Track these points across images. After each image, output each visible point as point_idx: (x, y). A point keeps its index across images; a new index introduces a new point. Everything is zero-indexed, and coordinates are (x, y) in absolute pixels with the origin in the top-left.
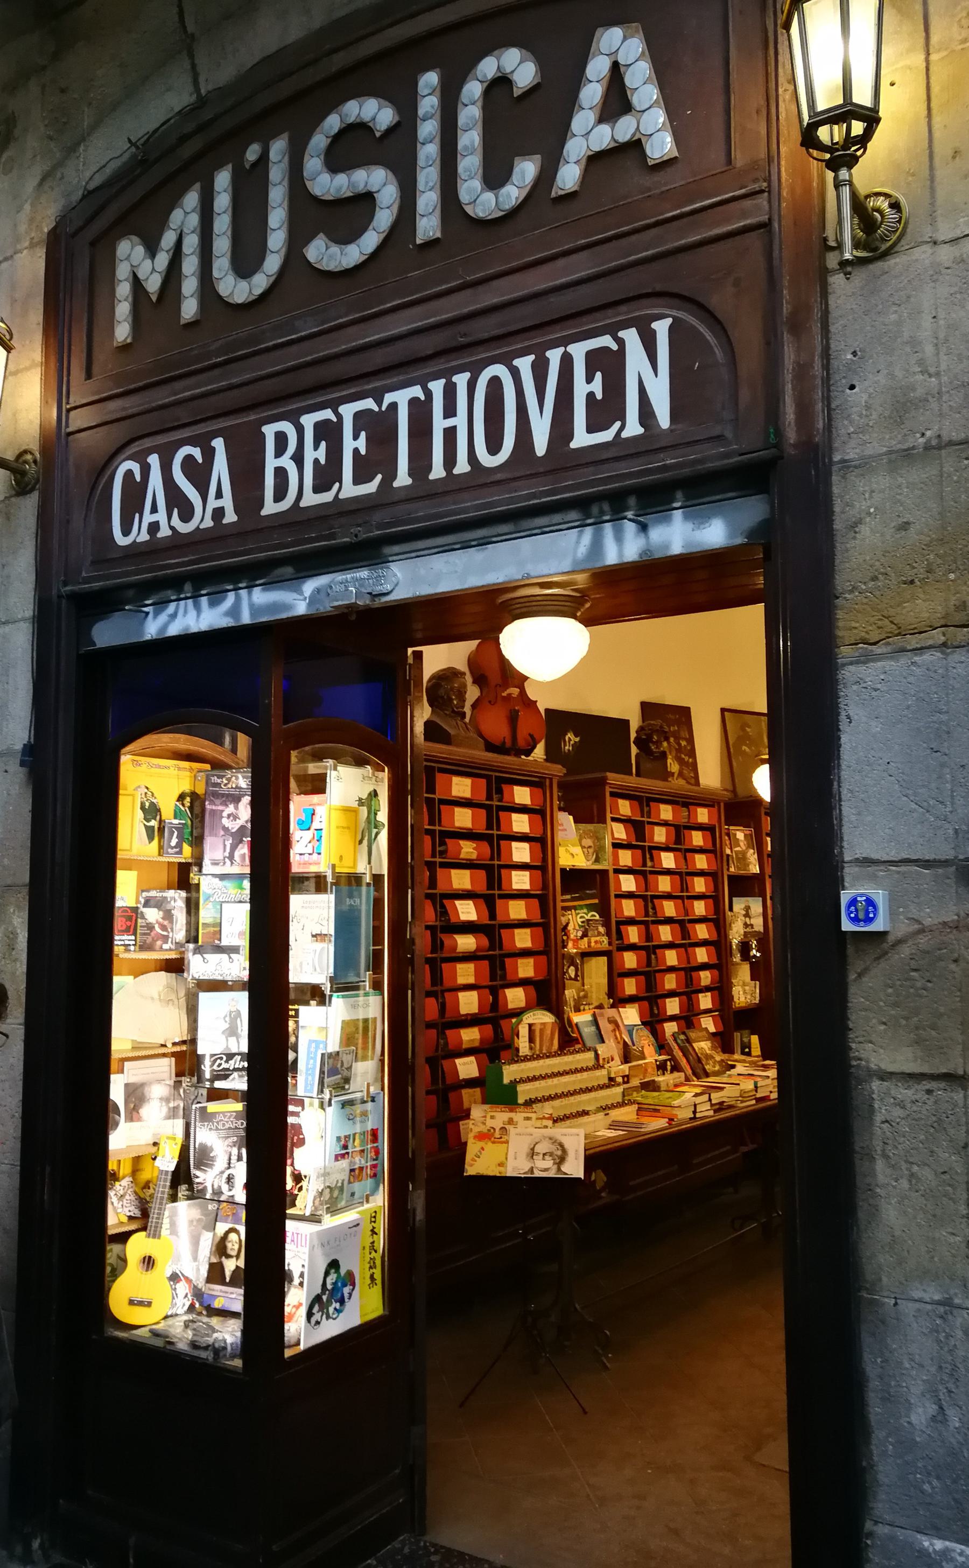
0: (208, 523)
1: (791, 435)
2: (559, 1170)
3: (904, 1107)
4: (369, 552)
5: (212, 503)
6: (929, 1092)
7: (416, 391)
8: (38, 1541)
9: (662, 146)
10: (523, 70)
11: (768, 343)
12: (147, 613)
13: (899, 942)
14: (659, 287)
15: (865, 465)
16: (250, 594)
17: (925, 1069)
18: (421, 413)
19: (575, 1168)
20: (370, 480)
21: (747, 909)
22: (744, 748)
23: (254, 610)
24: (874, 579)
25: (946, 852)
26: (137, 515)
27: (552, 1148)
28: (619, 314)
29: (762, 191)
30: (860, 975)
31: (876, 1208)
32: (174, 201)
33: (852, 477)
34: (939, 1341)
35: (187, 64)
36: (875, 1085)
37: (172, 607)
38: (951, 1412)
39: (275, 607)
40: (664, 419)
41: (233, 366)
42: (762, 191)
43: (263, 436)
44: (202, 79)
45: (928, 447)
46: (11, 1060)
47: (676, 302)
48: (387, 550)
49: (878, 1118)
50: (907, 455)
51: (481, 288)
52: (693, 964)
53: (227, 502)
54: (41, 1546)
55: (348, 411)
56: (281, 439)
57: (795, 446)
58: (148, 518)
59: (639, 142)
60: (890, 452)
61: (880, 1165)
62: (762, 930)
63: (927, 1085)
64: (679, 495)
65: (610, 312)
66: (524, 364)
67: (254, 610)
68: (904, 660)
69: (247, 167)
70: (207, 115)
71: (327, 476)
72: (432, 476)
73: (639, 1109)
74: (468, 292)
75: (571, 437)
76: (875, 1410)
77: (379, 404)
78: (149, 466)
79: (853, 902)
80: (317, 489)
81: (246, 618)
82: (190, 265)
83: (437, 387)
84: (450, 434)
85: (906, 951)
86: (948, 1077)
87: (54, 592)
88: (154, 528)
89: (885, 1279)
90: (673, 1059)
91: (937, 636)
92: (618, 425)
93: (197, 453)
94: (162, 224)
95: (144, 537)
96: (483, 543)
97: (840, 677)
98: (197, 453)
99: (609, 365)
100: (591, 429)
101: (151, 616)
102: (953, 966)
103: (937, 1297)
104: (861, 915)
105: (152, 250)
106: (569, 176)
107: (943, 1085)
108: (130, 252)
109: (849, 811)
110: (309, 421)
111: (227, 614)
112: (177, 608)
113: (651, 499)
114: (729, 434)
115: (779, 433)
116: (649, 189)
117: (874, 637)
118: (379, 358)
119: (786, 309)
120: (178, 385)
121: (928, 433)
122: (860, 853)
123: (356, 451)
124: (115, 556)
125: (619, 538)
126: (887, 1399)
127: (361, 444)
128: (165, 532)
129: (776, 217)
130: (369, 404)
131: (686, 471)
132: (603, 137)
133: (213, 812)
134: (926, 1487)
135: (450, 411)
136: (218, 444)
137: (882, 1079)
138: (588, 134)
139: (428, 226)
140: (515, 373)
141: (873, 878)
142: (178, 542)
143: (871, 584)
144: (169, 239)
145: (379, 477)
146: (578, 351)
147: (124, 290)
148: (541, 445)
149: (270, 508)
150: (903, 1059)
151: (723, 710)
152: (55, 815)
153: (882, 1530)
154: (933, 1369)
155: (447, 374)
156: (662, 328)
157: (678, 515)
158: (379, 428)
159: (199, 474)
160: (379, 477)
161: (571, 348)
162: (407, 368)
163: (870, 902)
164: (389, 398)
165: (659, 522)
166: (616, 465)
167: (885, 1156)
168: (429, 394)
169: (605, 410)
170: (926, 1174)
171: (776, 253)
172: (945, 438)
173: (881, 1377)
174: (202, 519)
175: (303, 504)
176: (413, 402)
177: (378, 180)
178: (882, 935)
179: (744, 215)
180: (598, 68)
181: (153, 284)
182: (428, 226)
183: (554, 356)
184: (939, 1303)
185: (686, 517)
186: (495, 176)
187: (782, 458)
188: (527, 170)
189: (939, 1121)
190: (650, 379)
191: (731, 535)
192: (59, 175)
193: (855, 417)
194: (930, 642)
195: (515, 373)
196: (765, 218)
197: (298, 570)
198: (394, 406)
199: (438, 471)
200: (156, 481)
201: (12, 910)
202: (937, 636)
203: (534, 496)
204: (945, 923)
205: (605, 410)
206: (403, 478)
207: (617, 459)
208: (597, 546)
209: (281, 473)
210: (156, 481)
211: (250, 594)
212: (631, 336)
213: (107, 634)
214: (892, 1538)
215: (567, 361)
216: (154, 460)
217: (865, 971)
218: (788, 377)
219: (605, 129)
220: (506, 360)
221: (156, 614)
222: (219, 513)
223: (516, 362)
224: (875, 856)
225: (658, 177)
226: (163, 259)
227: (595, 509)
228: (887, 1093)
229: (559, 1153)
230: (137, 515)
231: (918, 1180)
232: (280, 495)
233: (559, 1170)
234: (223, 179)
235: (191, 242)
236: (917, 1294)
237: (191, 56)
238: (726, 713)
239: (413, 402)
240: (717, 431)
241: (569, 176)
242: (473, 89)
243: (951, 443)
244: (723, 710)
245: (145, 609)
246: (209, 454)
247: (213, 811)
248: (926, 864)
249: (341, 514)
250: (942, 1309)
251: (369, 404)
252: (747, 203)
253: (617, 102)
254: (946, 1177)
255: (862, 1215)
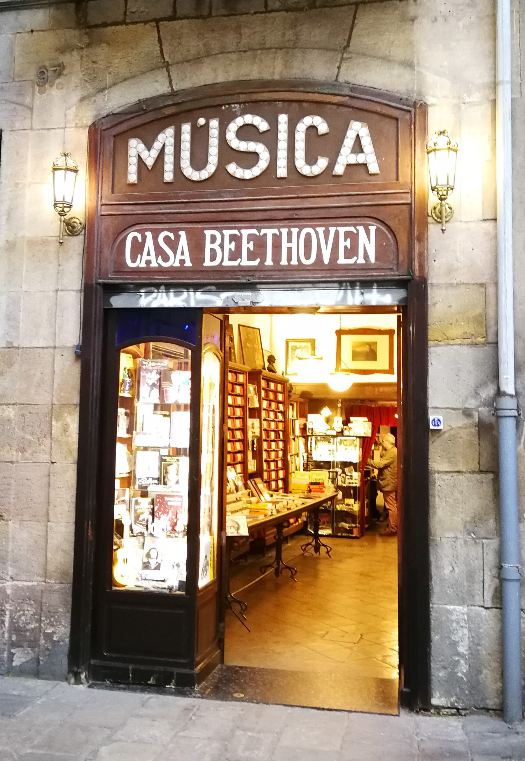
0: (177, 264)
1: (417, 273)
2: (238, 533)
3: (445, 481)
4: (251, 286)
5: (179, 257)
6: (452, 476)
7: (276, 231)
8: (84, 674)
9: (374, 168)
10: (323, 128)
11: (409, 242)
12: (141, 296)
13: (445, 432)
14: (372, 215)
15: (438, 286)
16: (195, 295)
17: (451, 470)
18: (277, 239)
19: (245, 532)
20: (255, 260)
21: (253, 424)
22: (248, 344)
23: (197, 301)
24: (441, 321)
25: (459, 406)
26: (139, 256)
27: (234, 524)
28: (357, 221)
29: (408, 193)
30: (433, 442)
31: (435, 512)
32: (161, 129)
33: (434, 288)
34: (453, 549)
35: (166, 74)
36: (436, 475)
37: (154, 295)
38: (456, 569)
39: (206, 301)
40: (372, 260)
41: (191, 204)
42: (408, 193)
43: (204, 235)
44: (174, 83)
45: (457, 284)
46: (66, 478)
47: (378, 221)
48: (258, 286)
49: (437, 485)
50: (451, 285)
51: (305, 199)
52: (236, 451)
53: (187, 257)
54: (86, 676)
55: (245, 233)
56: (213, 239)
57: (419, 277)
58: (145, 257)
59: (366, 164)
60: (446, 284)
61: (437, 499)
62: (259, 435)
63: (452, 474)
64: (375, 284)
65: (354, 219)
66: (321, 230)
67: (197, 301)
68: (449, 347)
69: (199, 127)
70: (178, 100)
71: (235, 255)
72: (282, 263)
73: (250, 511)
74: (299, 200)
75: (338, 259)
76: (434, 571)
77: (259, 233)
78: (146, 237)
79: (434, 420)
80: (230, 259)
81: (193, 304)
82: (169, 159)
83: (284, 231)
84: (289, 250)
85: (447, 435)
86: (458, 472)
87: (94, 282)
88: (148, 262)
89: (437, 532)
90: (252, 492)
91: (459, 341)
92: (355, 258)
93: (172, 235)
94: (154, 138)
95: (143, 265)
96: (300, 289)
97: (429, 350)
98: (172, 235)
99: (353, 237)
100: (346, 257)
101: (143, 297)
102: (460, 440)
103: (453, 536)
104: (436, 424)
105: (149, 147)
106: (339, 169)
107: (456, 474)
108: (135, 146)
109: (431, 392)
110: (227, 233)
111: (183, 301)
112: (157, 295)
113: (366, 285)
114: (395, 268)
115: (413, 272)
116: (369, 181)
117: (440, 339)
118: (260, 216)
119: (416, 233)
120: (161, 206)
121: (457, 280)
122: (434, 405)
123: (248, 249)
124: (126, 270)
125: (353, 295)
126: (437, 567)
127: (251, 246)
128: (154, 264)
129: (413, 202)
130: (254, 231)
131: (381, 278)
132: (353, 159)
133: (144, 376)
134: (448, 591)
135: (290, 240)
136: (182, 233)
137: (438, 473)
138: (346, 157)
139: (282, 172)
140: (317, 233)
141: (438, 413)
142: (160, 271)
143: (439, 323)
144: (157, 146)
145: (258, 260)
146: (342, 230)
147: (133, 161)
148: (326, 261)
149: (208, 263)
150: (446, 467)
151: (239, 325)
152: (93, 377)
153: (435, 606)
154: (451, 557)
155: (289, 227)
156: (373, 229)
157: (375, 291)
158: (260, 243)
159: (173, 245)
160: (258, 260)
161: (339, 229)
162: (271, 220)
163: (439, 420)
164: (263, 231)
165: (367, 292)
166: (354, 271)
167: (439, 496)
168: (281, 233)
169: (351, 252)
170: (451, 500)
171: (413, 214)
172: (462, 282)
173: (436, 562)
174: (174, 262)
175: (223, 264)
176: (274, 235)
177: (260, 148)
178: (440, 430)
179: (402, 199)
180: (351, 135)
181: (150, 162)
182: (282, 172)
183: (332, 230)
184: (453, 538)
185: (378, 292)
186: (311, 160)
187: (413, 279)
188: (322, 163)
189: (455, 485)
190: (368, 244)
191: (394, 300)
192: (93, 100)
193: (436, 271)
194: (457, 343)
195: (317, 233)
196: (409, 202)
197: (217, 289)
198: (265, 235)
199: (284, 262)
200: (149, 243)
201: (66, 415)
202: (459, 341)
203: (324, 277)
204: (458, 427)
205: (351, 252)
206: (269, 262)
207: (355, 270)
208: (345, 298)
209: (213, 251)
210: (149, 243)
211: (195, 295)
212: (361, 229)
213: (119, 302)
214: (438, 608)
215: (337, 233)
216: (149, 234)
217: (435, 440)
218: (416, 254)
219: (353, 156)
220: (313, 227)
221: (146, 296)
222: (182, 262)
223: (317, 229)
224: (438, 406)
225: (371, 178)
226: (154, 153)
227: (344, 284)
228: (440, 477)
229: (237, 526)
230: (139, 256)
231: (448, 502)
232: (213, 258)
233: (238, 533)
234: (186, 128)
235: (170, 150)
236: (447, 536)
237: (168, 71)
238: (241, 327)
239: (274, 235)
240: (391, 267)
241: (339, 169)
242: (301, 128)
243: (463, 284)
244: (239, 325)
245: (141, 294)
246: (178, 237)
247: (143, 376)
248: (454, 409)
249: (241, 271)
250: (454, 540)
251: (254, 231)
252: (403, 195)
253: (358, 148)
254: (456, 501)
255: (431, 514)
